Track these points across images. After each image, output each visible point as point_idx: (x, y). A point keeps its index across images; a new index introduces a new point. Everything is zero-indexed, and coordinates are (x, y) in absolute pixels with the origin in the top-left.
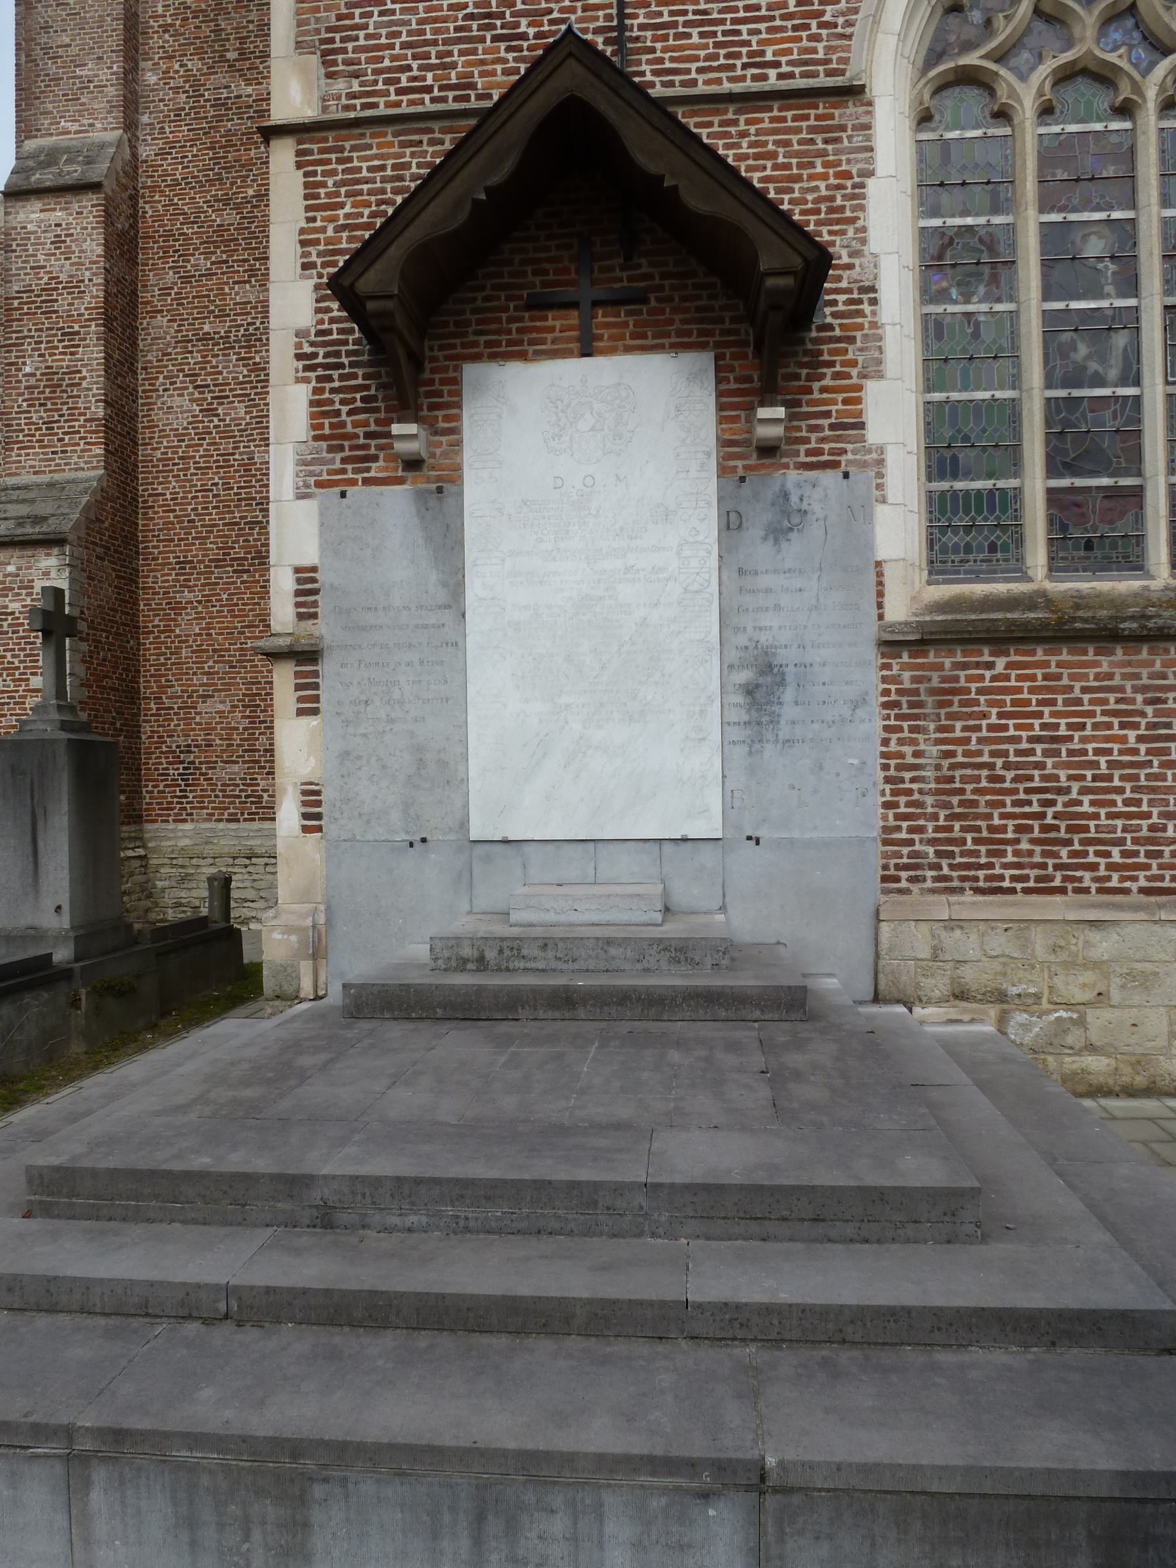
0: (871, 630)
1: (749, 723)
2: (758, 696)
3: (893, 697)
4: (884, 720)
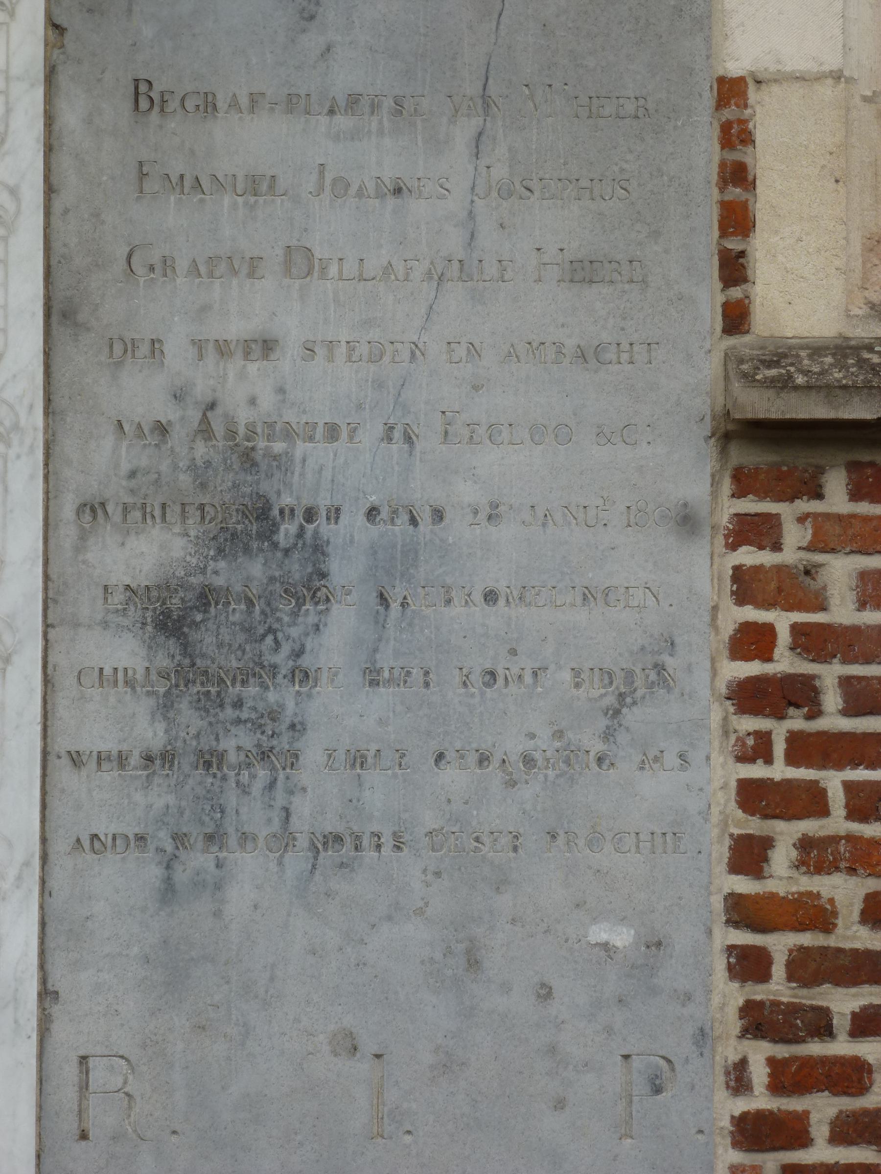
0: (694, 372)
1: (168, 757)
2: (206, 639)
3: (784, 662)
4: (743, 758)
